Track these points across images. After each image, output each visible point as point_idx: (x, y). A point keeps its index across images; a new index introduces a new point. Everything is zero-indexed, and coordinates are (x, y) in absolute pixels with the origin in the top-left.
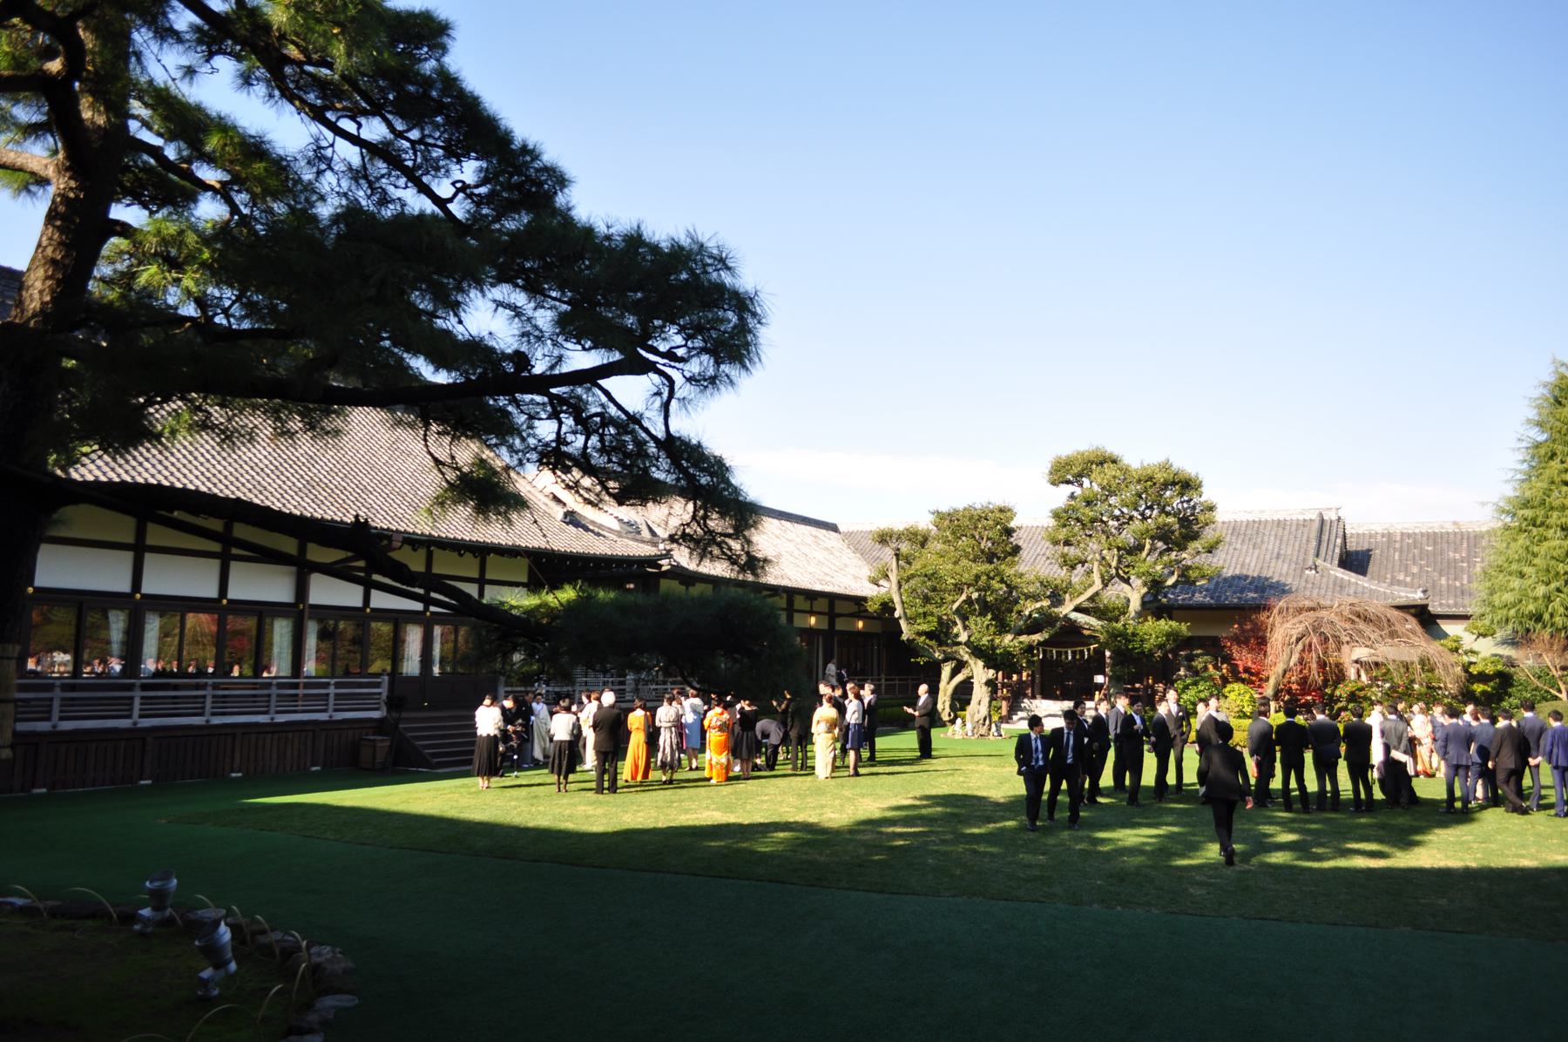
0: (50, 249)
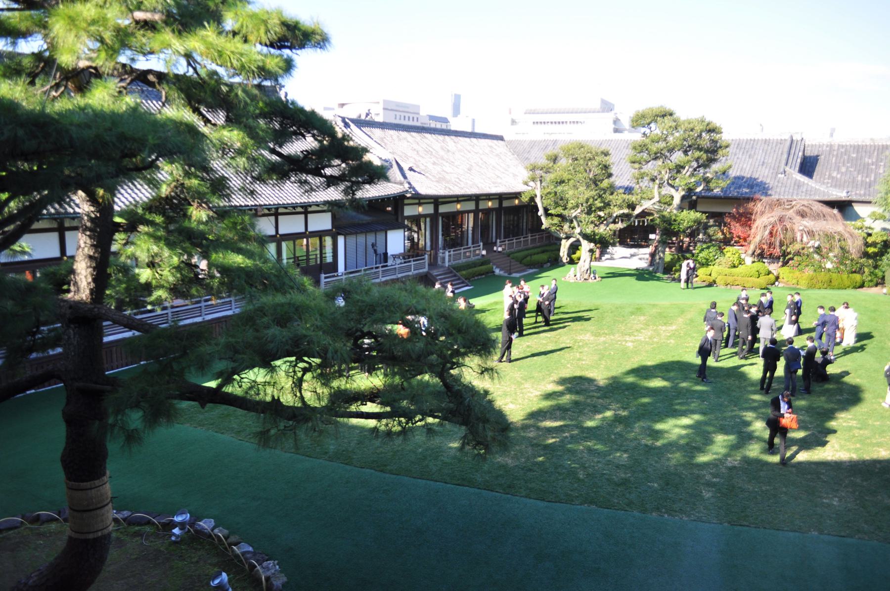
0: (86, 249)
